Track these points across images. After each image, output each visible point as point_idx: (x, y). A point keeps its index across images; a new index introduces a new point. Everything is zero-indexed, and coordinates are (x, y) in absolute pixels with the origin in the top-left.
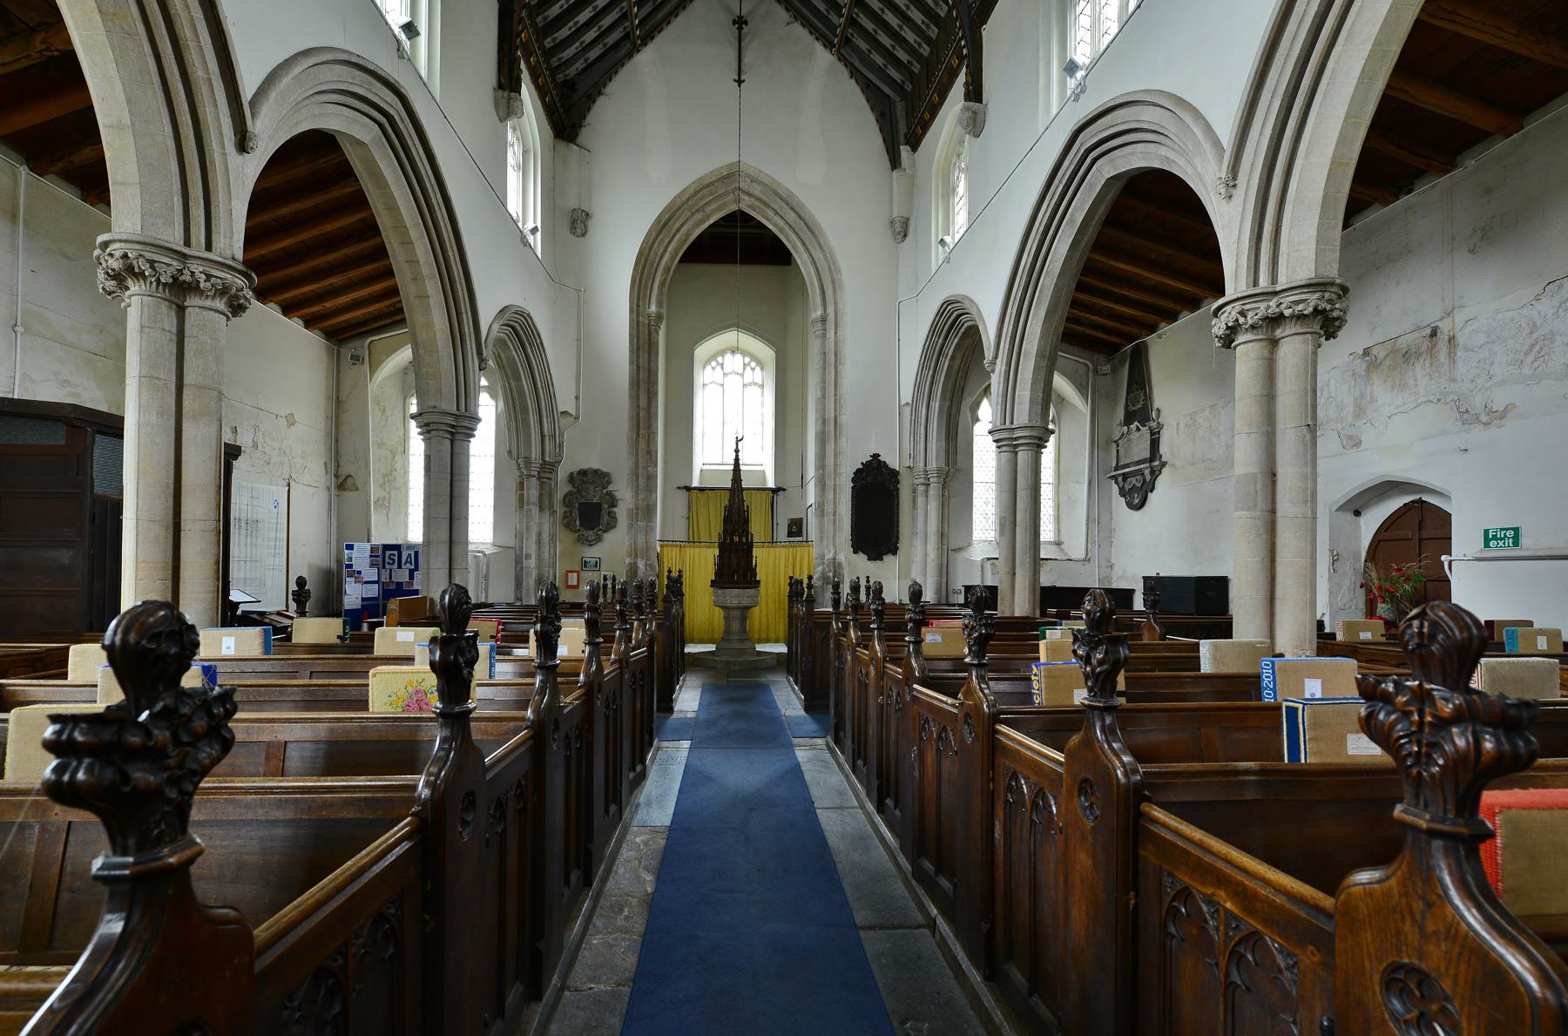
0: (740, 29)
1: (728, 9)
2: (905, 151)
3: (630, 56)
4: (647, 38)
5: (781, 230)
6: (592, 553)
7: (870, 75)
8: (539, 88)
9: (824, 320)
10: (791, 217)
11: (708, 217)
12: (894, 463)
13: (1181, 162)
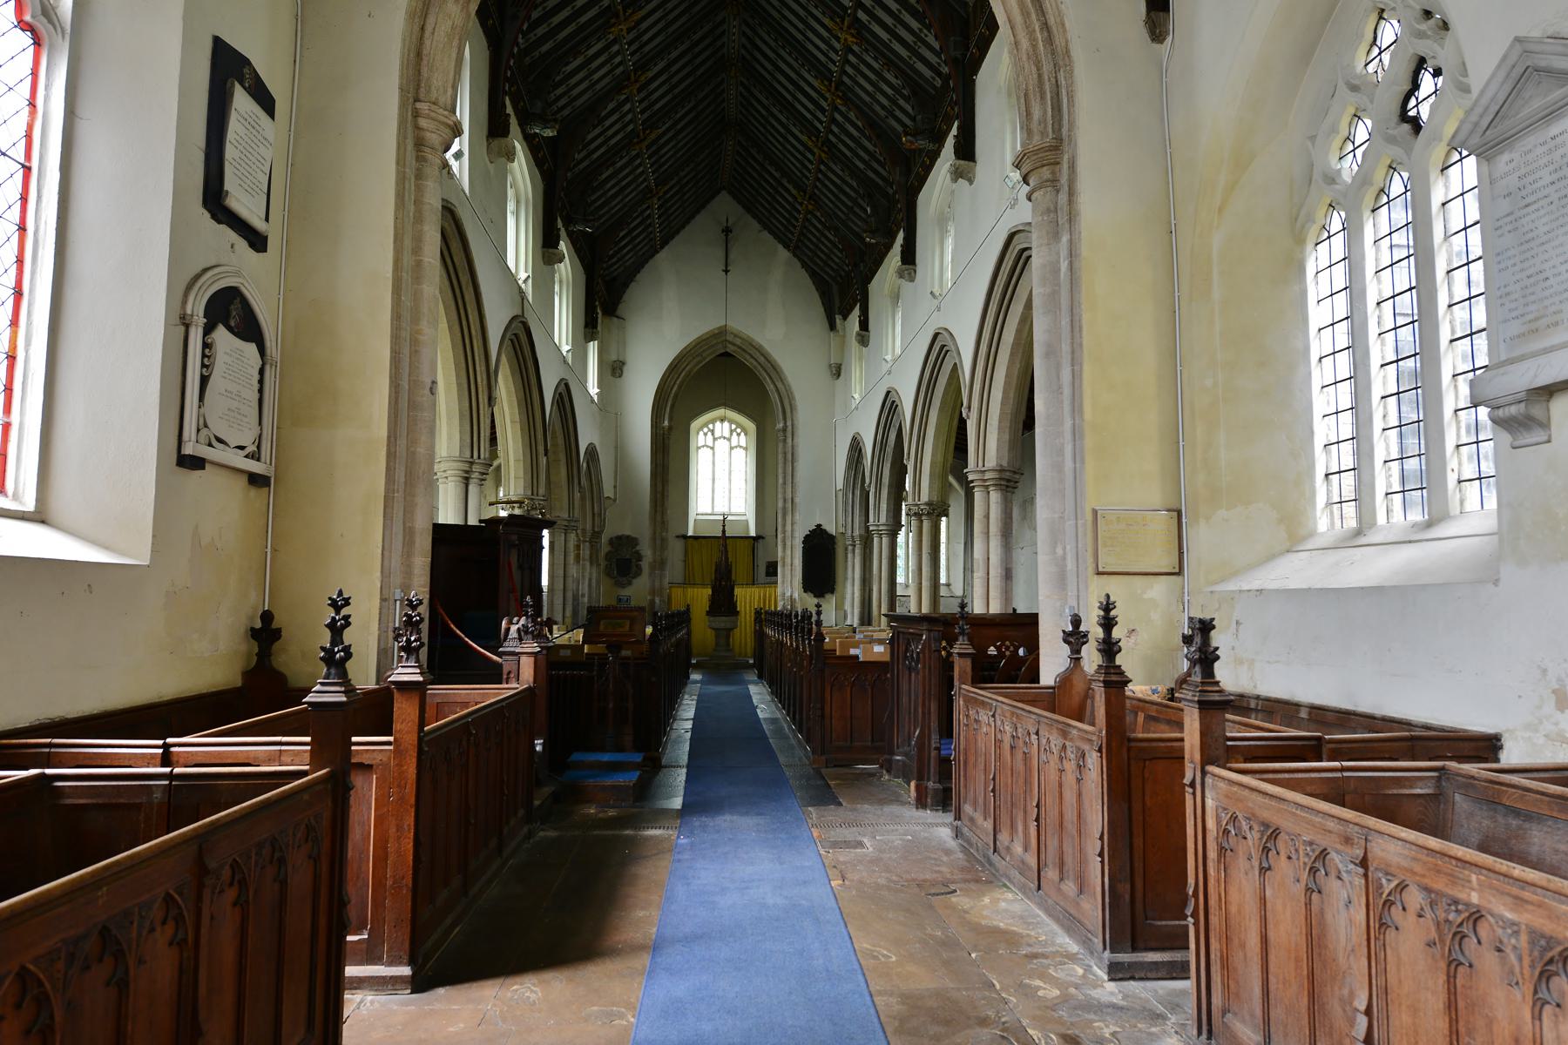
2: (838, 319)
6: (626, 592)
9: (784, 430)
10: (762, 359)
12: (831, 529)
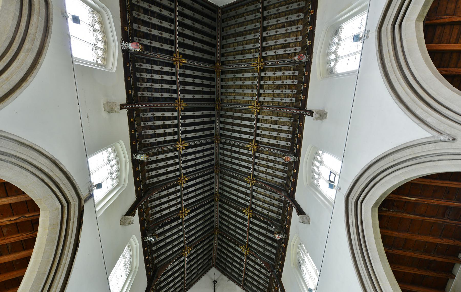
0: (215, 284)
1: (212, 279)
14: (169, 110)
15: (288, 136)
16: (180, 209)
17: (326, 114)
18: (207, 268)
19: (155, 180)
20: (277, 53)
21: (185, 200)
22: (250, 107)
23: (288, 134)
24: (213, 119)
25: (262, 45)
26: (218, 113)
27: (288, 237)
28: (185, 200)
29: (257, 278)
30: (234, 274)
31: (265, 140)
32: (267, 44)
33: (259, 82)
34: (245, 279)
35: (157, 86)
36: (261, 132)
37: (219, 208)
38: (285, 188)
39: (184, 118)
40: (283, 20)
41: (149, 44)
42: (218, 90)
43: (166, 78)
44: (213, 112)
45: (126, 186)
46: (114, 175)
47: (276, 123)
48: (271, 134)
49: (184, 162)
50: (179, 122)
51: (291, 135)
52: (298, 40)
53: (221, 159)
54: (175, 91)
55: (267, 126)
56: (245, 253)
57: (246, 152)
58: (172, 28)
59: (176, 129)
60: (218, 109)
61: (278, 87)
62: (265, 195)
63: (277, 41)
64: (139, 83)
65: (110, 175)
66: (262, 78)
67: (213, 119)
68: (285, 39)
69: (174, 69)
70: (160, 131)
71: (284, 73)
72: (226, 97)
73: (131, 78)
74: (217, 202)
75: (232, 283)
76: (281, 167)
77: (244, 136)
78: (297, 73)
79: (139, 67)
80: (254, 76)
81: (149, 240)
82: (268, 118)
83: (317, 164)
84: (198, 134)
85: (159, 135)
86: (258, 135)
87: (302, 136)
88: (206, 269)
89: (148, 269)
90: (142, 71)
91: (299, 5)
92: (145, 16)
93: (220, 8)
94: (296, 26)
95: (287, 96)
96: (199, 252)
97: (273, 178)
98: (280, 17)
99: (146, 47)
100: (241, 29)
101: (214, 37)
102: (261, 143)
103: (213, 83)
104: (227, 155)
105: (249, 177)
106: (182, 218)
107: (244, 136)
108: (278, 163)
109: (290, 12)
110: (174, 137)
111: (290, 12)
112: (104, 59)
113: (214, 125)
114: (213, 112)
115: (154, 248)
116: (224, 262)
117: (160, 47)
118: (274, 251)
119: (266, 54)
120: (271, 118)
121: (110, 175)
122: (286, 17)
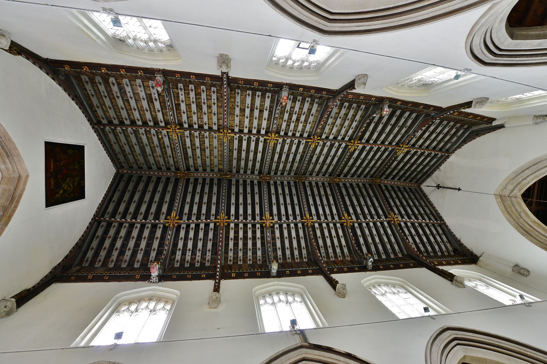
0: (441, 187)
1: (434, 190)
2: (494, 123)
3: (447, 226)
4: (441, 219)
5: (536, 177)
7: (460, 141)
8: (456, 263)
10: (528, 172)
11: (524, 211)
13: (502, 15)
14: (228, 233)
15: (258, 96)
16: (342, 225)
17: (221, 55)
18: (421, 194)
19: (304, 252)
20: (160, 109)
21: (333, 218)
22: (225, 140)
23: (257, 97)
24: (241, 182)
25: (151, 127)
26: (234, 176)
27: (387, 98)
28: (333, 218)
29: (441, 136)
30: (432, 163)
31: (264, 124)
32: (150, 121)
33: (196, 130)
34: (441, 150)
35: (200, 245)
36: (255, 128)
37: (348, 177)
38: (324, 100)
39: (237, 216)
40: (120, 102)
41: (155, 252)
42: (208, 176)
43: (191, 234)
44: (234, 182)
45: (304, 287)
46: (290, 299)
47: (243, 111)
48: (257, 117)
49: (288, 218)
50: (241, 222)
51: (257, 93)
52: (141, 84)
53: (289, 174)
54: (207, 225)
55: (247, 121)
56: (406, 150)
57: (279, 146)
58: (139, 226)
59: (249, 226)
60: (230, 176)
61: (199, 107)
62: (333, 124)
63: (145, 109)
64: (196, 264)
65: (288, 304)
66: (191, 126)
67: (241, 182)
68: (142, 100)
69: (182, 226)
70: (250, 243)
71: (182, 101)
72: (216, 166)
73: (189, 274)
74: (340, 179)
75: (443, 165)
76: (298, 104)
77: (260, 148)
78: (180, 85)
79: (179, 264)
80: (188, 135)
81: (371, 264)
82: (237, 120)
83: (290, 62)
84: (257, 200)
85: (254, 244)
86: (259, 131)
87: (256, 81)
88: (422, 195)
89: (407, 266)
90: (183, 260)
91: (100, 83)
92: (126, 255)
93: (117, 171)
94: (125, 86)
95: (209, 97)
96: (398, 204)
97: (312, 115)
98: (117, 106)
99: (157, 259)
100: (137, 148)
101: (150, 178)
102: (268, 128)
103: (200, 181)
104: (284, 166)
105: (310, 143)
106: (353, 223)
107: (260, 148)
108: (292, 107)
109: (110, 93)
110: (258, 228)
111: (110, 93)
112: (166, 302)
113: (248, 181)
114: (234, 182)
115: (384, 257)
116: (415, 173)
117: (158, 240)
118: (407, 114)
119: (161, 122)
120: (237, 116)
121: (288, 304)
122: (116, 98)
